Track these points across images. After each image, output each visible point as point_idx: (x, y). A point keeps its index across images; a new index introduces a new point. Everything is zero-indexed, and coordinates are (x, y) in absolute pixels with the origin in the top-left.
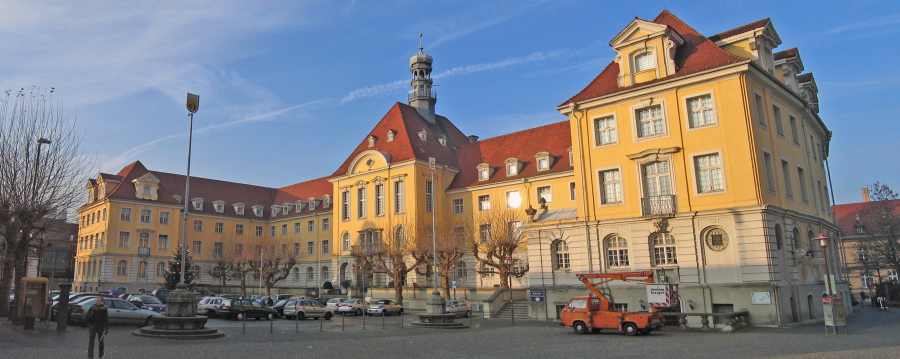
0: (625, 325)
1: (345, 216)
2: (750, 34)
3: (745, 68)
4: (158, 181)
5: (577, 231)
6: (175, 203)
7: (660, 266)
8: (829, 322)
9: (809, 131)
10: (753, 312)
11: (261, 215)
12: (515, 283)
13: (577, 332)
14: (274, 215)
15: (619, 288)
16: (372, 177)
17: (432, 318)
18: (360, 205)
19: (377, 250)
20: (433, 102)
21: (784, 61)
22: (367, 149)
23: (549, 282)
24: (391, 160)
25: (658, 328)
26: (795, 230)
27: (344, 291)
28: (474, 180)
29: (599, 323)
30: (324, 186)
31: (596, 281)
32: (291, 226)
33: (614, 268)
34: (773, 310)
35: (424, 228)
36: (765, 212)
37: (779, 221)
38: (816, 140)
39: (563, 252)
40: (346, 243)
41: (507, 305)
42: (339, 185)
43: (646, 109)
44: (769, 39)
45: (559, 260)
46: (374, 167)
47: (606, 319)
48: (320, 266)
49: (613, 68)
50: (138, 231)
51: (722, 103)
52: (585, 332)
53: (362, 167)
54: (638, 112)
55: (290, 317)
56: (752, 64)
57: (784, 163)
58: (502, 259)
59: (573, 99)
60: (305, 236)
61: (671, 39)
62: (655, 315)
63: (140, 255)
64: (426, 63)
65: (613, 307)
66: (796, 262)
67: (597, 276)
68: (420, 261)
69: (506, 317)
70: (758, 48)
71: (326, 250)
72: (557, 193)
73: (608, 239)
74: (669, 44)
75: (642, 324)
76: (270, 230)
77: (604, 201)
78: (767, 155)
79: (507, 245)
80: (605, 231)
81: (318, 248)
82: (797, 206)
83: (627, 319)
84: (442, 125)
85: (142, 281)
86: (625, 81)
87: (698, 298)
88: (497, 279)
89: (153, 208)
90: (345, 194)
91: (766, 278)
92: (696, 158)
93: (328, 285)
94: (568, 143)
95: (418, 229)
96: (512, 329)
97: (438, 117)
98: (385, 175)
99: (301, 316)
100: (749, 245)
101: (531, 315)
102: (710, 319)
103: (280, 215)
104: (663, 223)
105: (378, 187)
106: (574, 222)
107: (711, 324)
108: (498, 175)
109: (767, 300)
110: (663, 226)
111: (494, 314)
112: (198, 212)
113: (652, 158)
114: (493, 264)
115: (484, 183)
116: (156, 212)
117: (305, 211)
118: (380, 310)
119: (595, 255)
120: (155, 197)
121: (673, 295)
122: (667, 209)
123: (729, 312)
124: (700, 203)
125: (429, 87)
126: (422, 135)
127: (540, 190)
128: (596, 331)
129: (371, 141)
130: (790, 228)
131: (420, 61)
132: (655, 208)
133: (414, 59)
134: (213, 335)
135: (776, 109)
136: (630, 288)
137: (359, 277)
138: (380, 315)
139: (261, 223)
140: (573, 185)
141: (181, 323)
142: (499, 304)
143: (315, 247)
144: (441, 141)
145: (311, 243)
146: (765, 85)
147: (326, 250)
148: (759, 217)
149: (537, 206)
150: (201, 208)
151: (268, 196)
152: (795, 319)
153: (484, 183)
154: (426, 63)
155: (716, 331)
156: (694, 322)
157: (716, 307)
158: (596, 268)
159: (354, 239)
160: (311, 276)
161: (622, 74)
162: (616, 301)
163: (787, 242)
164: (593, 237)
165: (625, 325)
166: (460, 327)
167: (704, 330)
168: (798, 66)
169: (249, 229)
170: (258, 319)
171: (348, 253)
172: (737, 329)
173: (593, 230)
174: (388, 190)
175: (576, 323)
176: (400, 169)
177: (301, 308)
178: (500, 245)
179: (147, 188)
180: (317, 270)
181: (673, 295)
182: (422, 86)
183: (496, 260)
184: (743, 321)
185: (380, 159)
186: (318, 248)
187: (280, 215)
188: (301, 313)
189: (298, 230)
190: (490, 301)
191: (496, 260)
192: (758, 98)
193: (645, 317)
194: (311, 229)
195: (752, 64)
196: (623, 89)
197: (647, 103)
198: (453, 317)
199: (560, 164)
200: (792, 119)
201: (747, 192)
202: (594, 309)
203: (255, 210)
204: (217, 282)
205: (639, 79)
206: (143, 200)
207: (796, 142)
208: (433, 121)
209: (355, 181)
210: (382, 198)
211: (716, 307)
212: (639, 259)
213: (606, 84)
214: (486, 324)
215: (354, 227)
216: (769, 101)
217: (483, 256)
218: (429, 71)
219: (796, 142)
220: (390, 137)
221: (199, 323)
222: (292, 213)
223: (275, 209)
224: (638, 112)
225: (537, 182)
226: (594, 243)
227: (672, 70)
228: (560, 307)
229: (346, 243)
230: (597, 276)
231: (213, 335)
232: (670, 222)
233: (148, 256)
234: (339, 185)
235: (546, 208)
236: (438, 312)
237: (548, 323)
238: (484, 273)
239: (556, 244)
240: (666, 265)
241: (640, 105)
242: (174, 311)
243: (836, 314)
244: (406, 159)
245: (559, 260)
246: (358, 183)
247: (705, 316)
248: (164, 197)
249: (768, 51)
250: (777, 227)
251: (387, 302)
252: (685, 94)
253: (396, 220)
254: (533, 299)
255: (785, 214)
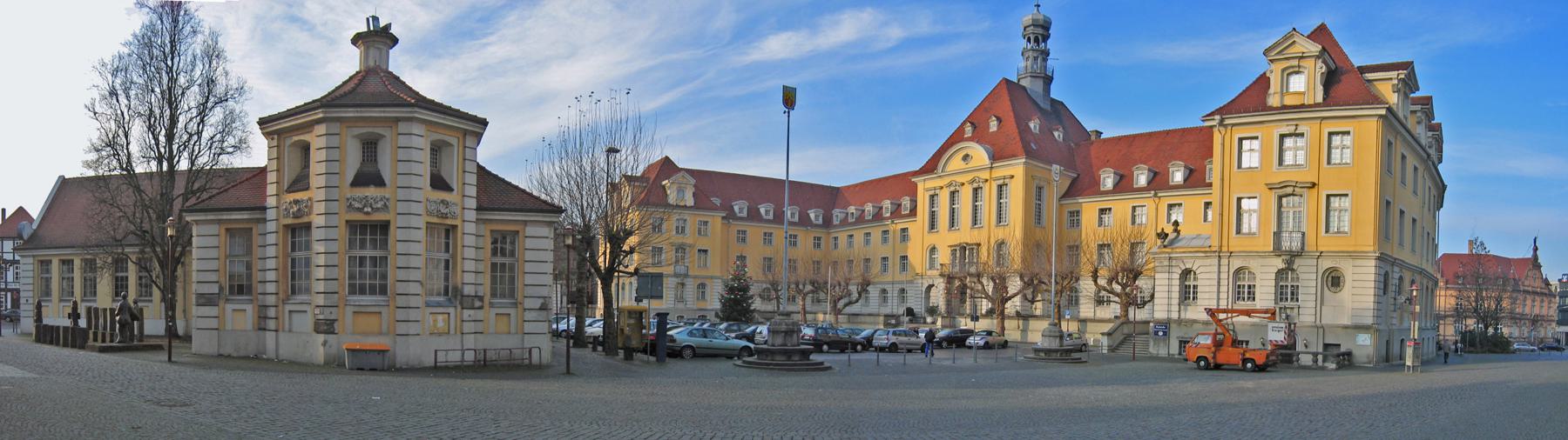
0: (1245, 361)
1: (932, 226)
2: (1393, 74)
3: (1383, 112)
4: (693, 181)
5: (1208, 261)
6: (714, 208)
7: (1282, 304)
8: (1409, 363)
9: (1429, 183)
10: (1356, 352)
11: (820, 221)
12: (1141, 315)
13: (1200, 368)
14: (836, 222)
15: (1243, 324)
16: (970, 177)
17: (1048, 351)
18: (952, 211)
19: (973, 270)
20: (1048, 80)
21: (1418, 107)
22: (962, 140)
23: (1175, 316)
24: (996, 157)
25: (1274, 364)
26: (1401, 278)
27: (929, 320)
28: (1094, 188)
29: (1221, 359)
30: (903, 184)
31: (1222, 316)
32: (859, 236)
33: (1241, 305)
34: (1371, 351)
35: (1034, 246)
36: (1378, 258)
37: (1388, 268)
38: (1434, 192)
39: (1192, 283)
40: (932, 261)
41: (1127, 338)
42: (924, 186)
43: (1290, 135)
44: (1409, 84)
45: (1188, 294)
46: (972, 164)
47: (1230, 355)
48: (898, 287)
49: (1263, 81)
50: (672, 244)
51: (1357, 142)
52: (1207, 368)
53: (956, 163)
54: (1282, 137)
55: (882, 349)
56: (1389, 109)
57: (1402, 212)
58: (1124, 286)
59: (1220, 111)
60: (877, 249)
61: (1324, 62)
62: (1272, 352)
63: (676, 275)
64: (1042, 27)
65: (1236, 343)
66: (1396, 307)
67: (1224, 311)
68: (1027, 285)
69: (1126, 350)
70: (1398, 91)
71: (904, 267)
72: (1189, 213)
73: (1238, 271)
74: (1321, 68)
75: (1260, 361)
76: (832, 242)
77: (1238, 232)
78: (1388, 203)
79: (1131, 271)
80: (1236, 263)
81: (894, 263)
82: (1405, 255)
83: (1247, 356)
84: (1058, 112)
85: (680, 306)
86: (1273, 101)
87: (1312, 339)
88: (1114, 310)
89: (686, 215)
90: (932, 197)
91: (1369, 321)
92: (1328, 196)
93: (910, 312)
94: (1209, 153)
95: (1025, 245)
96: (1134, 364)
97: (1055, 103)
98: (985, 175)
99: (893, 348)
100: (1360, 292)
101: (1152, 350)
102: (1320, 357)
103: (844, 223)
104: (1292, 256)
105: (975, 190)
106: (1207, 252)
107: (1320, 363)
108: (1124, 185)
109: (1368, 342)
110: (1289, 268)
111: (1112, 349)
112: (741, 219)
113: (1289, 190)
114: (1112, 292)
115: (1107, 193)
116: (692, 220)
117: (878, 217)
118: (982, 343)
119: (1224, 289)
120: (690, 201)
121: (1291, 333)
122: (1296, 245)
123: (1335, 351)
124: (1327, 243)
125: (1045, 60)
126: (1034, 125)
127: (1171, 206)
128: (1218, 367)
129: (968, 129)
130: (1397, 276)
131: (1035, 24)
132: (1285, 245)
133: (1028, 19)
134: (820, 368)
135: (1403, 157)
136: (1254, 325)
137: (948, 303)
138: (979, 348)
139: (820, 233)
140: (1207, 205)
141: (788, 354)
142: (1119, 337)
143: (890, 262)
144: (1056, 134)
145: (885, 259)
146: (1398, 133)
147: (904, 267)
148: (1373, 263)
149: (1169, 229)
150: (745, 214)
151: (829, 196)
152: (1387, 360)
153: (1107, 193)
154: (1042, 27)
155: (1323, 368)
156: (1306, 360)
157: (1326, 346)
158: (1223, 305)
159: (944, 256)
160: (885, 300)
161: (1271, 91)
162: (1240, 338)
163: (1392, 288)
164: (1224, 269)
165: (1245, 361)
166: (1078, 361)
167: (1315, 368)
168: (1429, 115)
169: (805, 239)
170: (842, 351)
171: (936, 273)
172: (1340, 367)
173: (1224, 261)
174: (988, 193)
175: (1199, 359)
176: (1003, 169)
177: (893, 339)
178: (1123, 270)
179: (680, 190)
180: (893, 293)
181: (1291, 333)
182: (1036, 59)
183: (1118, 288)
184: (1346, 361)
185: (980, 154)
186: (894, 263)
187: (844, 223)
188: (894, 344)
189: (867, 242)
190: (1109, 334)
191: (1118, 288)
192: (1390, 144)
193: (1264, 354)
194: (885, 240)
195: (1389, 109)
196: (1272, 108)
197: (1291, 129)
198: (1071, 351)
199: (1196, 179)
200: (1416, 169)
201: (1367, 239)
202: (1218, 345)
203: (812, 216)
204: (770, 307)
205: (1289, 101)
206: (678, 206)
207: (1415, 192)
208: (1048, 108)
209: (946, 181)
210: (982, 207)
211: (1326, 346)
212: (1265, 296)
213: (1253, 99)
214: (1104, 359)
215: (945, 240)
216: (1400, 148)
217: (1102, 282)
218: (1046, 38)
219: (1415, 192)
220: (993, 125)
221: (805, 354)
222: (860, 219)
223: (837, 214)
224: (1282, 137)
225: (1167, 198)
226: (1224, 276)
227: (1320, 99)
228: (1183, 343)
229: (932, 261)
230: (1224, 311)
231: (820, 368)
232: (1298, 262)
233: (686, 276)
234: (924, 186)
235: (1176, 231)
236: (1055, 344)
237: (1170, 358)
238: (1099, 302)
239: (1186, 273)
240: (1289, 304)
241: (1285, 130)
242: (779, 340)
243: (1415, 356)
244: (1013, 156)
245: (1188, 294)
246: (950, 185)
247: (1315, 355)
248: (701, 203)
249: (1406, 96)
250: (1386, 274)
251: (989, 333)
252: (1329, 127)
253: (1000, 234)
254: (1156, 333)
255: (1394, 262)
